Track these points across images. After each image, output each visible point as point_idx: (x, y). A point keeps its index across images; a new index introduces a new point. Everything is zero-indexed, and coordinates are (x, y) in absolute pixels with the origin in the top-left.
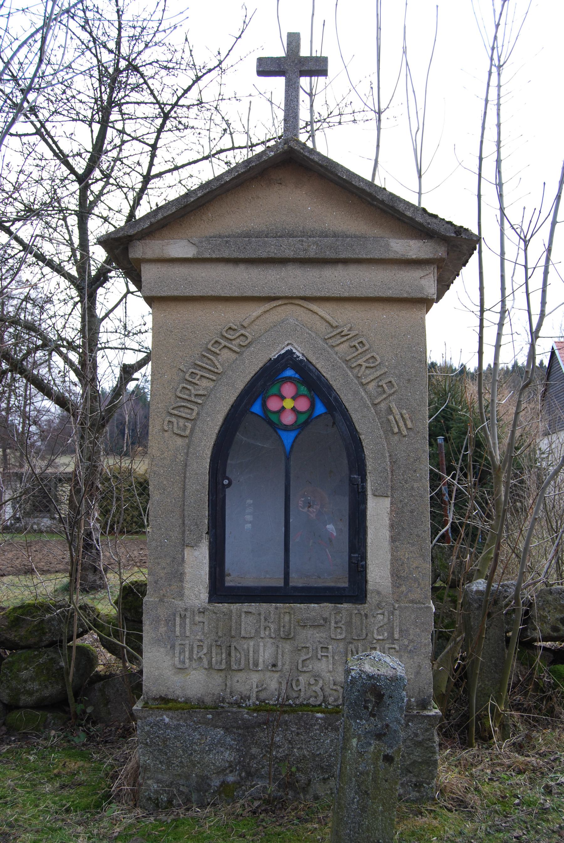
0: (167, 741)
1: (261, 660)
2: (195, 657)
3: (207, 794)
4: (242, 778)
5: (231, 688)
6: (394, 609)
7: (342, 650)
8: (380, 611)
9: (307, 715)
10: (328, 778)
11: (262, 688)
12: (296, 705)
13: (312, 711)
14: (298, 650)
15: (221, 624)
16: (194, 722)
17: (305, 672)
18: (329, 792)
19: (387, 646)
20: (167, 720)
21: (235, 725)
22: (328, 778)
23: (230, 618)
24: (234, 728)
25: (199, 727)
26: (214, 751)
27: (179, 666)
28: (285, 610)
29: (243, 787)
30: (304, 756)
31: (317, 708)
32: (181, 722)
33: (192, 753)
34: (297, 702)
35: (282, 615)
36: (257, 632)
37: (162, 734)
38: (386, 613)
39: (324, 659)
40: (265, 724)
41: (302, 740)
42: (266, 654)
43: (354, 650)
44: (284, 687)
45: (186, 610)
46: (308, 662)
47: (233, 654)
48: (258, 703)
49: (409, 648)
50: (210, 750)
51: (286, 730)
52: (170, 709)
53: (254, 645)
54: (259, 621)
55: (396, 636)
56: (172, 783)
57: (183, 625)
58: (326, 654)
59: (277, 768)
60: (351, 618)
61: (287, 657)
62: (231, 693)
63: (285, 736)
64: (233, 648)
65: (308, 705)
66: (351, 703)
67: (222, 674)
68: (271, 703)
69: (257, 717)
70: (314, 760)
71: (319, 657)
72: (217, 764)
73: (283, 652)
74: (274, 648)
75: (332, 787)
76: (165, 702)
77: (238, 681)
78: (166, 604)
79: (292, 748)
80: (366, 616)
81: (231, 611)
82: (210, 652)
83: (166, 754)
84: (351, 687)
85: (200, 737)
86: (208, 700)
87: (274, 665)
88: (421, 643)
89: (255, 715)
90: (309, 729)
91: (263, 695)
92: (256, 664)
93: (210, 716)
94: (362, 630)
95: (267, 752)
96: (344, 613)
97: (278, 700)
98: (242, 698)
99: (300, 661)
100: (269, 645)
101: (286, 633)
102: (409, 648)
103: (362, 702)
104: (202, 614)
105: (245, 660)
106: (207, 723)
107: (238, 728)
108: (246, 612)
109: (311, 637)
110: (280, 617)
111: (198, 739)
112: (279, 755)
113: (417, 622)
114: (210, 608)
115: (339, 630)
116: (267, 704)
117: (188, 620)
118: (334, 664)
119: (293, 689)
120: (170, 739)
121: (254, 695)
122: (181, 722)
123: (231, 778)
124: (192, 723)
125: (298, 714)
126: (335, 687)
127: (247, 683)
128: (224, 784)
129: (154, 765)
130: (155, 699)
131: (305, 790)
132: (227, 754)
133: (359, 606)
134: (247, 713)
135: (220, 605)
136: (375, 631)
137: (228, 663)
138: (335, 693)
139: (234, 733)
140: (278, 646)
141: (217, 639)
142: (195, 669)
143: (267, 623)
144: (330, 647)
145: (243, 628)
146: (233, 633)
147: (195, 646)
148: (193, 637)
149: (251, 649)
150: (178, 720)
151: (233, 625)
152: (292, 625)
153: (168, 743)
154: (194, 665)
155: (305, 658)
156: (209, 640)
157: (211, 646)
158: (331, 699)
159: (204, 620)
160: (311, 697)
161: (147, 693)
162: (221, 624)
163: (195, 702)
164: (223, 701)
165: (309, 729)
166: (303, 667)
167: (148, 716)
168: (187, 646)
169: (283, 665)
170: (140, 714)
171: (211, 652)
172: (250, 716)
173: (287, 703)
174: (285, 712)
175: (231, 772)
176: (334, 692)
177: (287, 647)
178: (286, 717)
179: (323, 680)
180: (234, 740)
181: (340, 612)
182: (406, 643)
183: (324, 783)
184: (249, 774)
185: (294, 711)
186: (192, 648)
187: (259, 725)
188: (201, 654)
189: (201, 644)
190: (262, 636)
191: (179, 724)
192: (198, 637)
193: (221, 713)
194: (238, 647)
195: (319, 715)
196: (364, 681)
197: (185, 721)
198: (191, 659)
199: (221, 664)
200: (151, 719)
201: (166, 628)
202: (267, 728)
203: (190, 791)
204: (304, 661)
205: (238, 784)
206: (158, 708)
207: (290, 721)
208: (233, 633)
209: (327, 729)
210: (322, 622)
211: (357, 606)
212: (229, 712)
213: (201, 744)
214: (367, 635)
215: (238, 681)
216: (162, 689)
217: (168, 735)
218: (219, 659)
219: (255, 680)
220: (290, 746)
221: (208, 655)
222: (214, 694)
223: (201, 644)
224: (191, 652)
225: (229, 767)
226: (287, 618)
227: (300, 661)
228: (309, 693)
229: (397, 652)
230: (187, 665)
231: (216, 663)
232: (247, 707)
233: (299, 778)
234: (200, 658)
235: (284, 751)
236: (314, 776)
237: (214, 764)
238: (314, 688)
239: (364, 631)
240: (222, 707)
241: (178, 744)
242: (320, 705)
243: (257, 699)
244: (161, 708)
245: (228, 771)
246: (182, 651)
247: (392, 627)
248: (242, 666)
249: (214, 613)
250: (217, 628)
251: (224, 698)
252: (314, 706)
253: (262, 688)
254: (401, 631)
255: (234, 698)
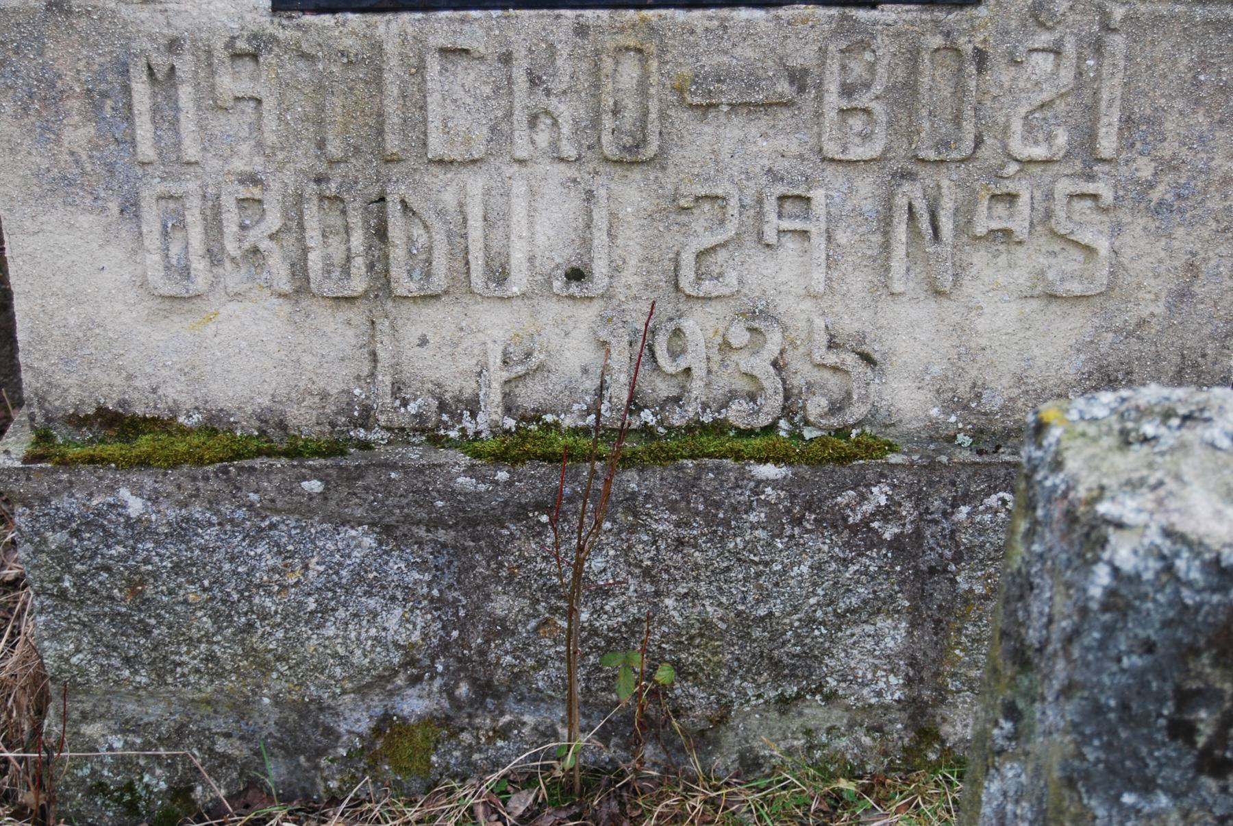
0: (143, 582)
1: (518, 258)
2: (231, 247)
3: (323, 762)
4: (457, 704)
5: (396, 367)
6: (1107, 28)
7: (867, 206)
8: (1044, 39)
9: (718, 470)
10: (799, 697)
11: (523, 362)
12: (670, 428)
13: (738, 456)
14: (678, 209)
15: (336, 105)
16: (251, 506)
17: (707, 299)
18: (800, 743)
19: (1064, 187)
20: (135, 506)
21: (422, 514)
22: (799, 697)
23: (376, 80)
24: (418, 523)
25: (273, 526)
26: (341, 613)
27: (168, 289)
28: (622, 40)
29: (466, 737)
30: (706, 623)
31: (762, 442)
32: (197, 511)
33: (250, 626)
34: (677, 420)
35: (608, 64)
36: (499, 133)
37: (122, 558)
38: (1070, 48)
39: (790, 244)
40: (540, 507)
41: (696, 566)
42: (540, 225)
43: (921, 206)
44: (620, 360)
45: (173, 45)
46: (722, 255)
47: (396, 231)
48: (510, 423)
49: (1155, 195)
50: (324, 610)
51: (632, 529)
52: (143, 463)
53: (488, 192)
54: (505, 88)
55: (1107, 144)
56: (180, 730)
57: (168, 113)
58: (798, 225)
59: (597, 668)
60: (914, 70)
61: (632, 241)
62: (397, 388)
63: (626, 552)
64: (394, 208)
65: (719, 428)
66: (1098, 710)
67: (357, 314)
68: (568, 422)
69: (510, 483)
70: (746, 636)
71: (771, 236)
72: (357, 658)
73: (613, 215)
74: (575, 203)
75: (812, 724)
76: (122, 432)
77: (423, 342)
78: (82, 24)
79: (657, 594)
80: (981, 58)
81: (378, 47)
82: (295, 223)
83: (147, 632)
84: (1109, 631)
85: (278, 562)
86: (304, 419)
87: (576, 275)
88: (1209, 171)
89: (502, 475)
90: (726, 523)
91: (531, 395)
92: (499, 274)
93: (315, 486)
94: (957, 120)
95: (554, 610)
96: (885, 47)
97: (595, 409)
98: (442, 407)
99: (688, 259)
100: (552, 189)
101: (628, 141)
102: (1155, 195)
103: (1161, 700)
104: (249, 65)
105: (452, 255)
106: (305, 508)
107: (434, 523)
108: (444, 51)
109: (734, 151)
110: (597, 69)
111: (273, 570)
112: (603, 623)
113: (1198, 84)
114: (281, 34)
115: (857, 123)
116: (548, 427)
117: (185, 94)
118: (831, 262)
119: (657, 368)
120: (155, 575)
121: (496, 396)
122: (197, 511)
123: (414, 704)
124: (240, 514)
125: (681, 468)
126: (832, 359)
127: (461, 350)
128: (387, 726)
129: (104, 671)
130: (77, 421)
131: (705, 740)
132: (393, 619)
133: (952, 17)
134: (470, 470)
135: (327, 19)
136: (1017, 126)
137: (379, 269)
138: (833, 382)
139: (420, 543)
140: (590, 196)
141: (322, 168)
142: (237, 296)
143: (540, 98)
144: (818, 195)
145: (434, 123)
146: (392, 143)
147: (229, 202)
148: (215, 164)
149: (475, 213)
150: (184, 505)
151: (392, 108)
152: (654, 107)
153: (149, 591)
154: (232, 278)
155: (708, 241)
156: (288, 176)
157: (300, 199)
158: (816, 407)
159: (262, 91)
160: (732, 396)
161: (42, 400)
162: (336, 105)
163: (246, 427)
164: (366, 418)
165: (726, 523)
166: (699, 278)
167: (57, 493)
168: (194, 203)
169: (615, 270)
170: (20, 488)
171: (301, 227)
172: (482, 479)
173: (636, 423)
174: (628, 461)
175: (415, 680)
176: (827, 374)
177: (631, 194)
178: (631, 480)
179: (785, 329)
180: (422, 566)
181: (864, 46)
182: (1146, 173)
183: (783, 713)
184: (485, 690)
185: (667, 457)
186: (217, 210)
187: (520, 513)
188: (258, 236)
189: (256, 192)
190: (521, 154)
191: (187, 520)
192: (239, 165)
193: (360, 472)
194: (415, 202)
195: (769, 471)
196: (1189, 598)
197: (213, 503)
198: (214, 256)
199: (346, 272)
200: (67, 504)
201: (91, 130)
202: (553, 521)
203: (257, 753)
204: (701, 255)
205: (444, 725)
206: (92, 460)
207: (648, 497)
208: (392, 143)
209: (798, 521)
210: (784, 87)
211: (939, 14)
212: (394, 467)
213: (284, 588)
214: (979, 142)
215: (423, 342)
216: (105, 379)
217: (147, 561)
218: (337, 250)
219: (498, 334)
220: (649, 588)
221: (289, 240)
222: (324, 396)
223: (256, 192)
224: (213, 224)
225: (404, 665)
226: (629, 71)
227: (688, 259)
228: (725, 381)
229: (1105, 210)
230: (200, 282)
231: (327, 272)
232: (468, 444)
233: (685, 702)
234: (256, 251)
235: (623, 608)
236: (742, 693)
237: (344, 661)
238: (745, 362)
239: (969, 128)
240: (365, 445)
241: (192, 593)
242: (771, 428)
243: (508, 410)
244: (104, 461)
245: (400, 681)
246: (173, 226)
247: (1092, 109)
248: (439, 281)
249: (304, 56)
250: (320, 123)
251: (367, 411)
252: (743, 433)
253: (523, 362)
254: (1128, 121)
255: (412, 408)
